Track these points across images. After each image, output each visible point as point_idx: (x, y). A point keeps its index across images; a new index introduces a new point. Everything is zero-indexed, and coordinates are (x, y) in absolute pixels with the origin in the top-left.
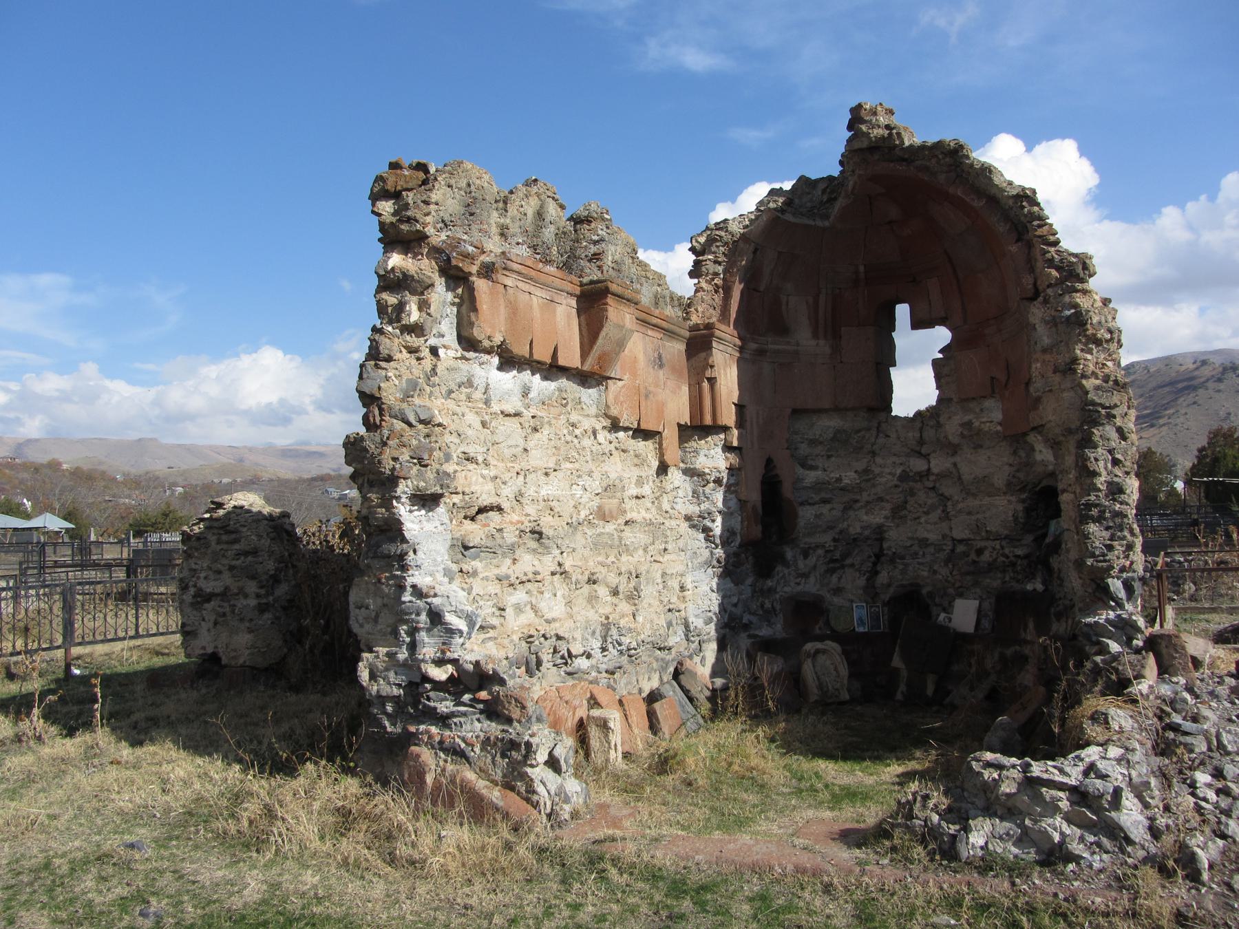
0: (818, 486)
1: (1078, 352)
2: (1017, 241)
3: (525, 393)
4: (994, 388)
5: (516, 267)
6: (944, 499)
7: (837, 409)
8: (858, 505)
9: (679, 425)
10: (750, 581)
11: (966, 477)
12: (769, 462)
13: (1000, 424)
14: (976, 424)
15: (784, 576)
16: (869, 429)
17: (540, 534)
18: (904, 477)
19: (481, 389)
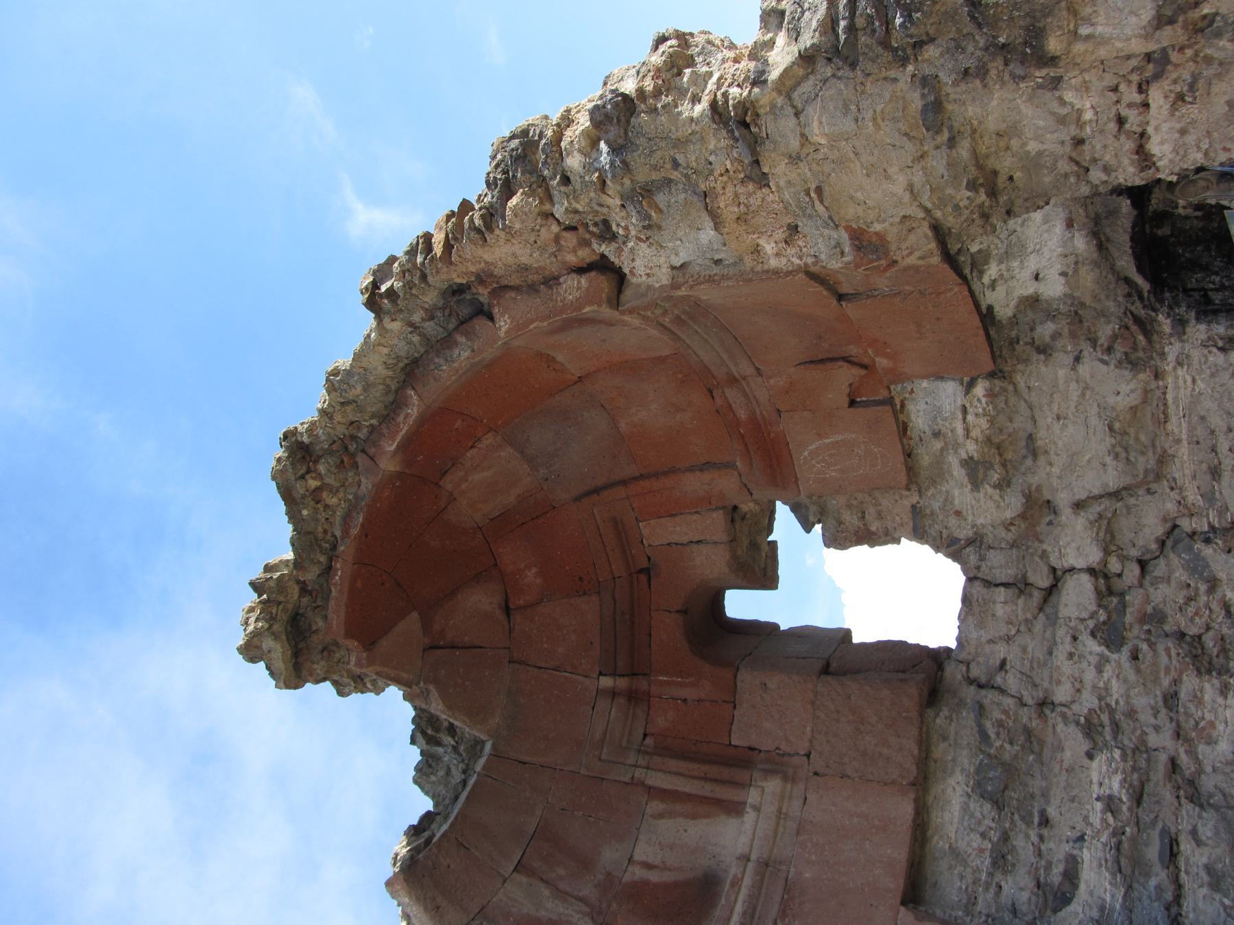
0: (1126, 864)
1: (698, 109)
2: (491, 318)
4: (876, 398)
6: (1171, 537)
7: (922, 782)
8: (1184, 759)
11: (1113, 478)
13: (971, 385)
14: (971, 448)
16: (981, 709)
18: (1111, 634)
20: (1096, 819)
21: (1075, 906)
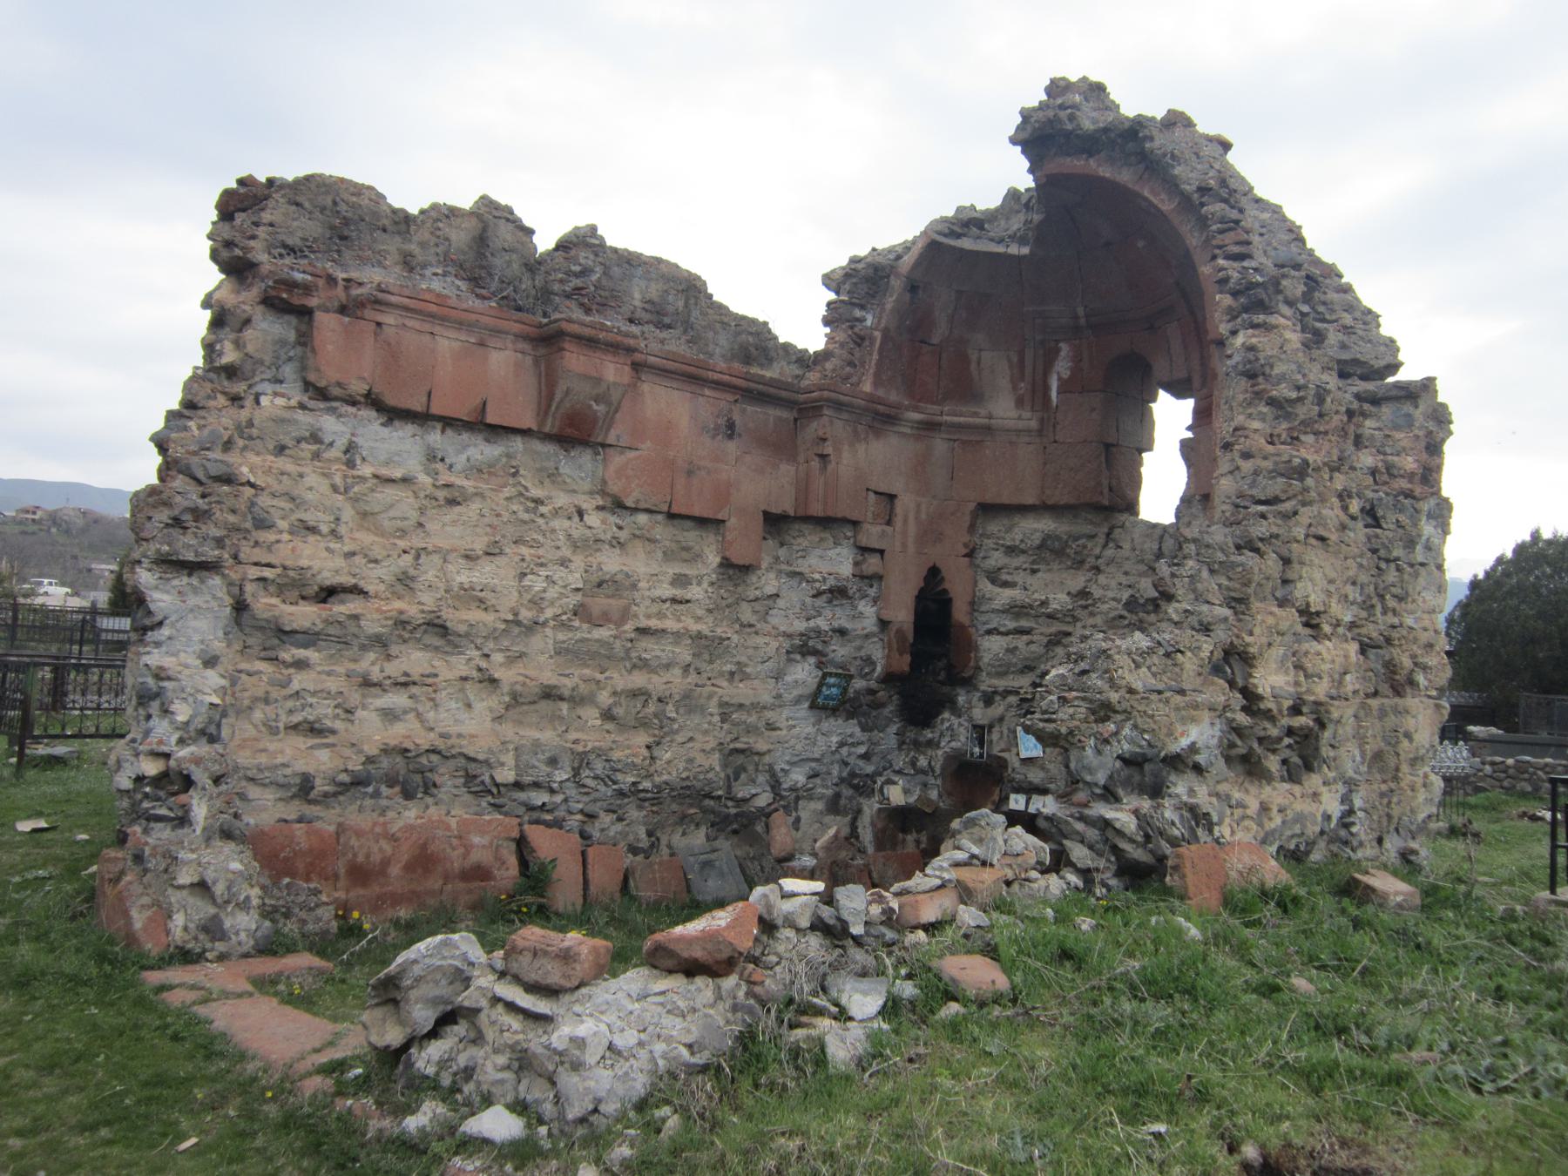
0: (1016, 610)
3: (432, 457)
5: (393, 299)
9: (765, 513)
10: (893, 728)
12: (934, 574)
15: (950, 728)
16: (1092, 537)
17: (444, 627)
19: (341, 443)
20: (1036, 596)
21: (990, 586)
